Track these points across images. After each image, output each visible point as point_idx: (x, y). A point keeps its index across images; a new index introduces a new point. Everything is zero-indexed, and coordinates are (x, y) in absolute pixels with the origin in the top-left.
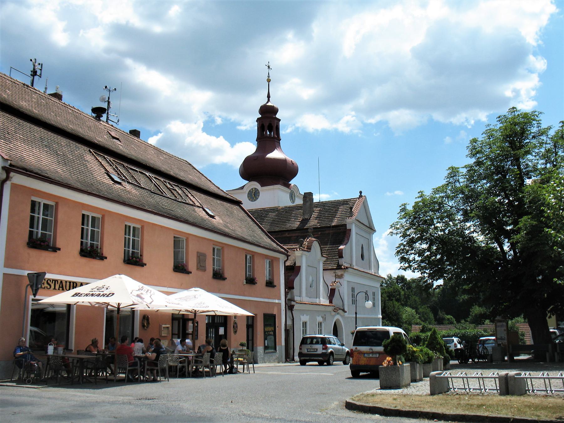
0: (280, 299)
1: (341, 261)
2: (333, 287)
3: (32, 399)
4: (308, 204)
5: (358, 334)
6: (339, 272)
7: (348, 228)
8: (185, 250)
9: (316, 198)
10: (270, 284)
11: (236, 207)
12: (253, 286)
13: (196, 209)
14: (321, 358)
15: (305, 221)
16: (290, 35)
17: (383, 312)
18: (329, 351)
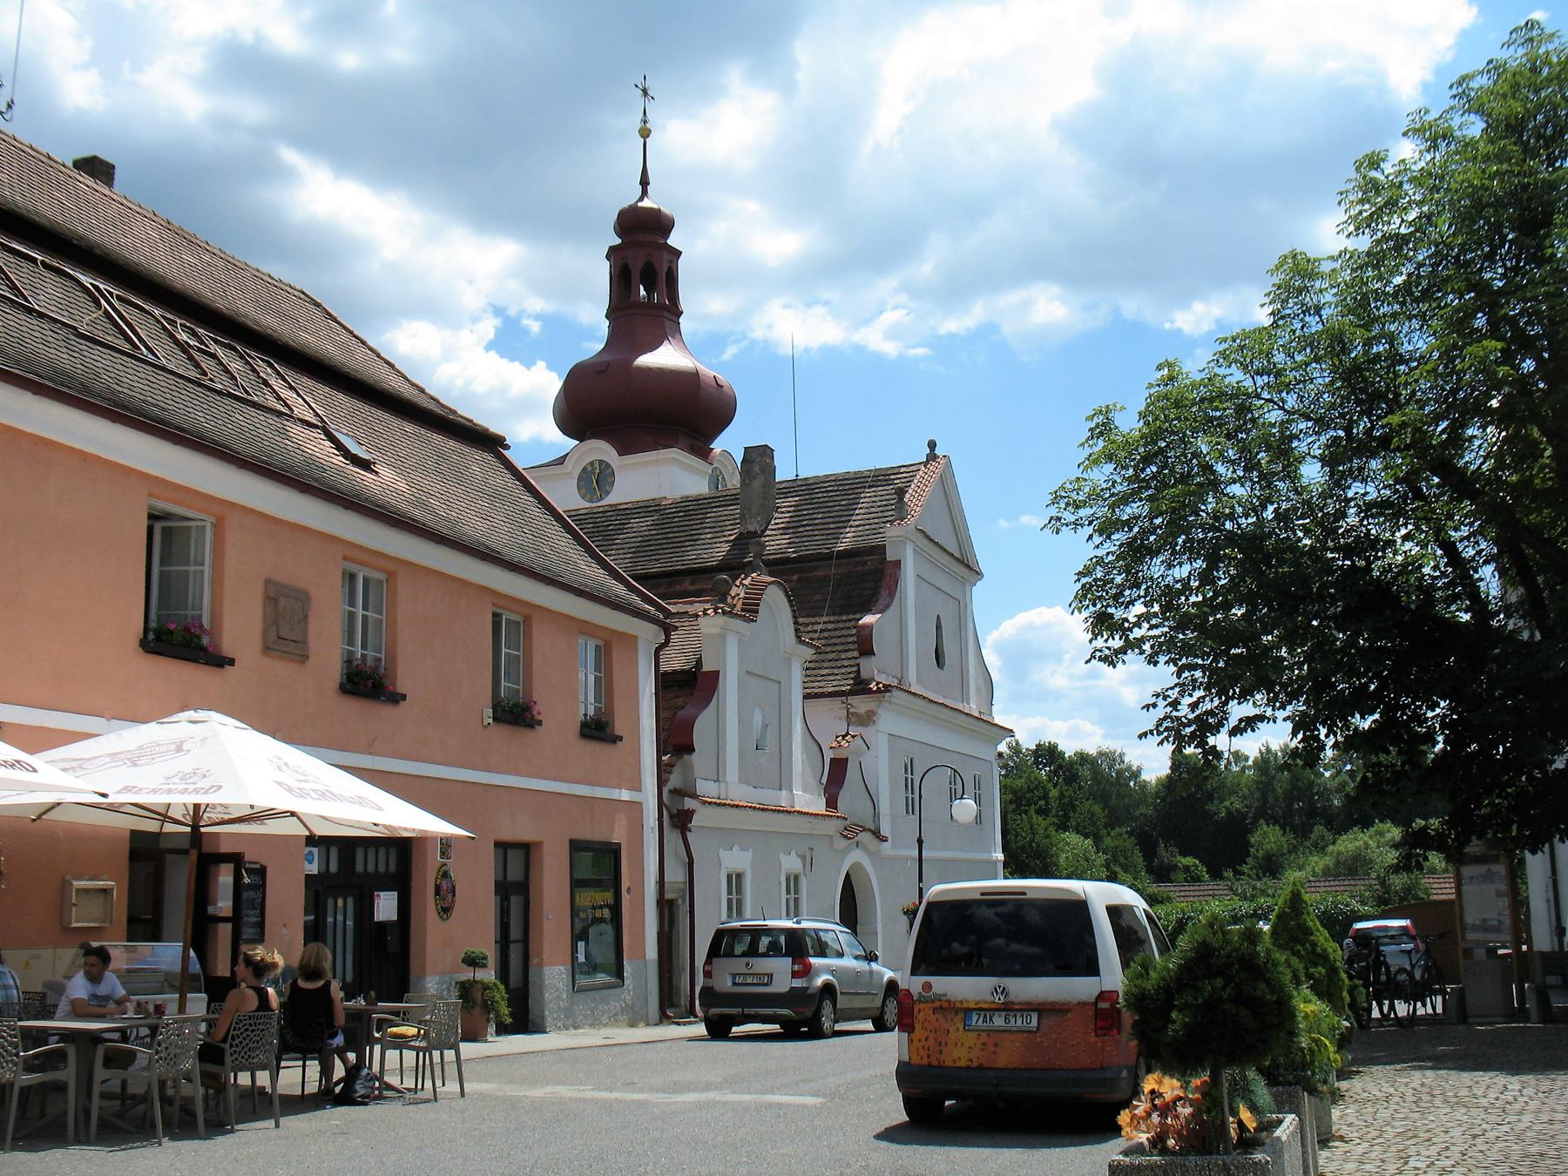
0: (636, 786)
1: (869, 667)
2: (840, 754)
4: (757, 484)
5: (935, 917)
6: (861, 704)
7: (891, 556)
8: (207, 569)
9: (784, 471)
10: (597, 730)
11: (477, 461)
12: (526, 735)
13: (295, 430)
14: (786, 1012)
15: (745, 541)
17: (1006, 848)
18: (819, 981)
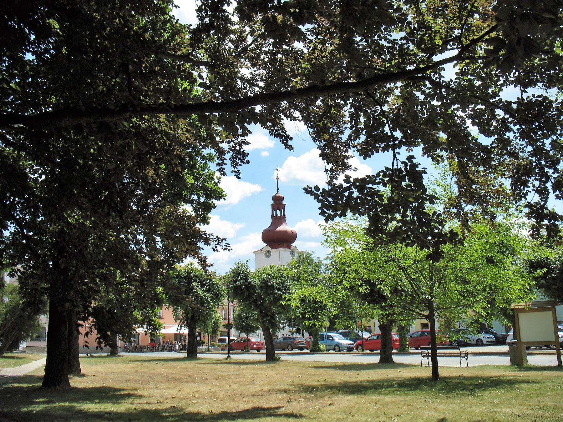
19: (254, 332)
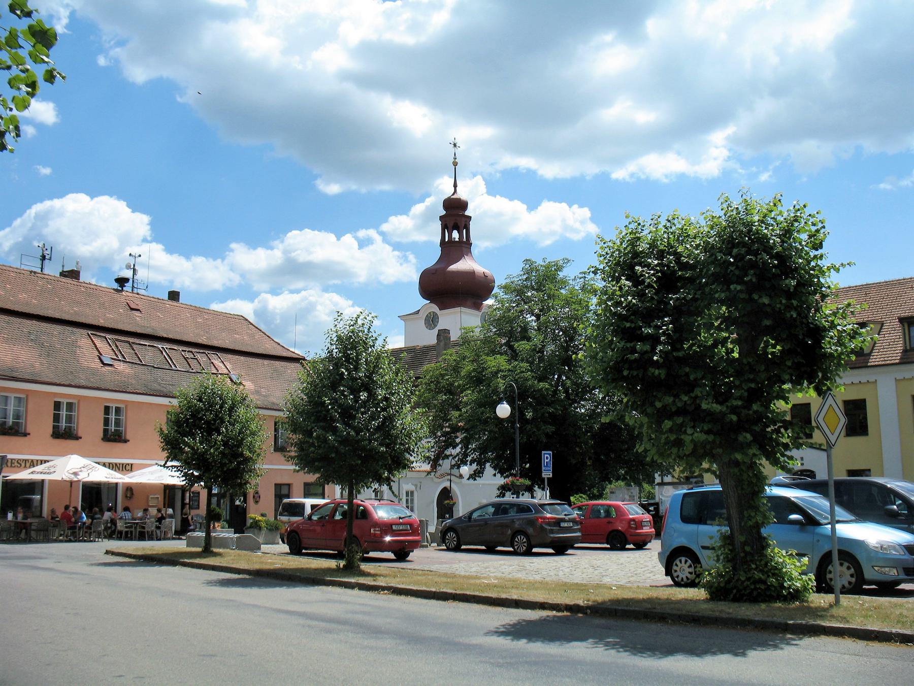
3: (366, 643)
16: (609, 37)
19: (380, 480)
